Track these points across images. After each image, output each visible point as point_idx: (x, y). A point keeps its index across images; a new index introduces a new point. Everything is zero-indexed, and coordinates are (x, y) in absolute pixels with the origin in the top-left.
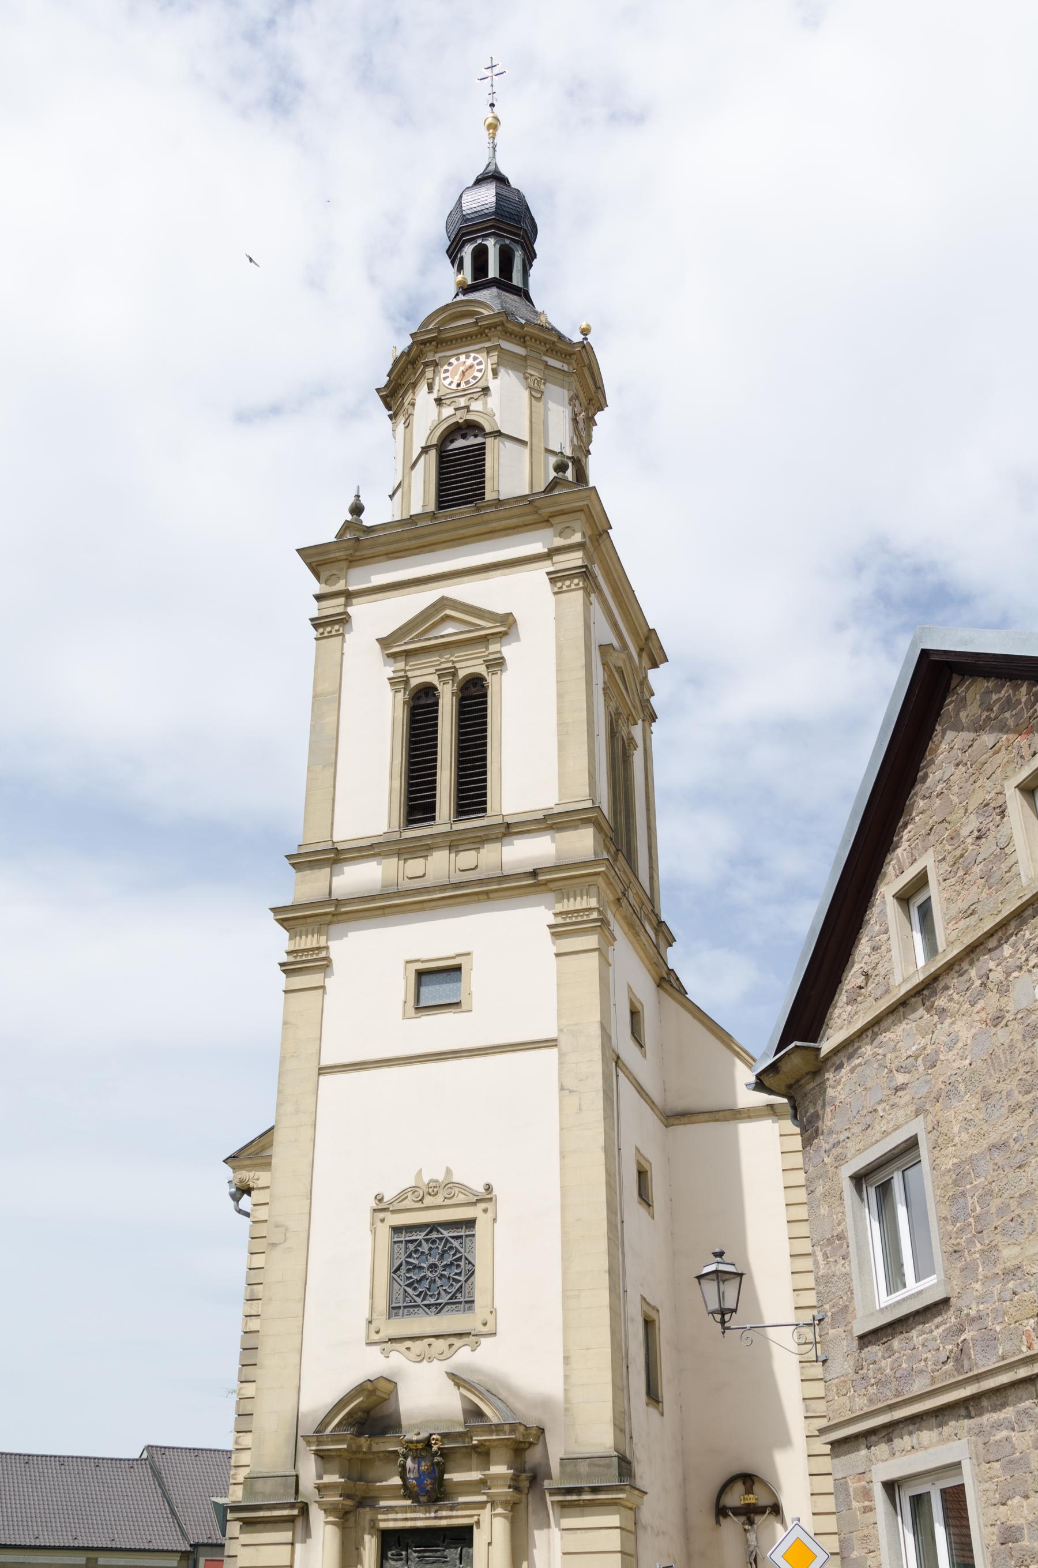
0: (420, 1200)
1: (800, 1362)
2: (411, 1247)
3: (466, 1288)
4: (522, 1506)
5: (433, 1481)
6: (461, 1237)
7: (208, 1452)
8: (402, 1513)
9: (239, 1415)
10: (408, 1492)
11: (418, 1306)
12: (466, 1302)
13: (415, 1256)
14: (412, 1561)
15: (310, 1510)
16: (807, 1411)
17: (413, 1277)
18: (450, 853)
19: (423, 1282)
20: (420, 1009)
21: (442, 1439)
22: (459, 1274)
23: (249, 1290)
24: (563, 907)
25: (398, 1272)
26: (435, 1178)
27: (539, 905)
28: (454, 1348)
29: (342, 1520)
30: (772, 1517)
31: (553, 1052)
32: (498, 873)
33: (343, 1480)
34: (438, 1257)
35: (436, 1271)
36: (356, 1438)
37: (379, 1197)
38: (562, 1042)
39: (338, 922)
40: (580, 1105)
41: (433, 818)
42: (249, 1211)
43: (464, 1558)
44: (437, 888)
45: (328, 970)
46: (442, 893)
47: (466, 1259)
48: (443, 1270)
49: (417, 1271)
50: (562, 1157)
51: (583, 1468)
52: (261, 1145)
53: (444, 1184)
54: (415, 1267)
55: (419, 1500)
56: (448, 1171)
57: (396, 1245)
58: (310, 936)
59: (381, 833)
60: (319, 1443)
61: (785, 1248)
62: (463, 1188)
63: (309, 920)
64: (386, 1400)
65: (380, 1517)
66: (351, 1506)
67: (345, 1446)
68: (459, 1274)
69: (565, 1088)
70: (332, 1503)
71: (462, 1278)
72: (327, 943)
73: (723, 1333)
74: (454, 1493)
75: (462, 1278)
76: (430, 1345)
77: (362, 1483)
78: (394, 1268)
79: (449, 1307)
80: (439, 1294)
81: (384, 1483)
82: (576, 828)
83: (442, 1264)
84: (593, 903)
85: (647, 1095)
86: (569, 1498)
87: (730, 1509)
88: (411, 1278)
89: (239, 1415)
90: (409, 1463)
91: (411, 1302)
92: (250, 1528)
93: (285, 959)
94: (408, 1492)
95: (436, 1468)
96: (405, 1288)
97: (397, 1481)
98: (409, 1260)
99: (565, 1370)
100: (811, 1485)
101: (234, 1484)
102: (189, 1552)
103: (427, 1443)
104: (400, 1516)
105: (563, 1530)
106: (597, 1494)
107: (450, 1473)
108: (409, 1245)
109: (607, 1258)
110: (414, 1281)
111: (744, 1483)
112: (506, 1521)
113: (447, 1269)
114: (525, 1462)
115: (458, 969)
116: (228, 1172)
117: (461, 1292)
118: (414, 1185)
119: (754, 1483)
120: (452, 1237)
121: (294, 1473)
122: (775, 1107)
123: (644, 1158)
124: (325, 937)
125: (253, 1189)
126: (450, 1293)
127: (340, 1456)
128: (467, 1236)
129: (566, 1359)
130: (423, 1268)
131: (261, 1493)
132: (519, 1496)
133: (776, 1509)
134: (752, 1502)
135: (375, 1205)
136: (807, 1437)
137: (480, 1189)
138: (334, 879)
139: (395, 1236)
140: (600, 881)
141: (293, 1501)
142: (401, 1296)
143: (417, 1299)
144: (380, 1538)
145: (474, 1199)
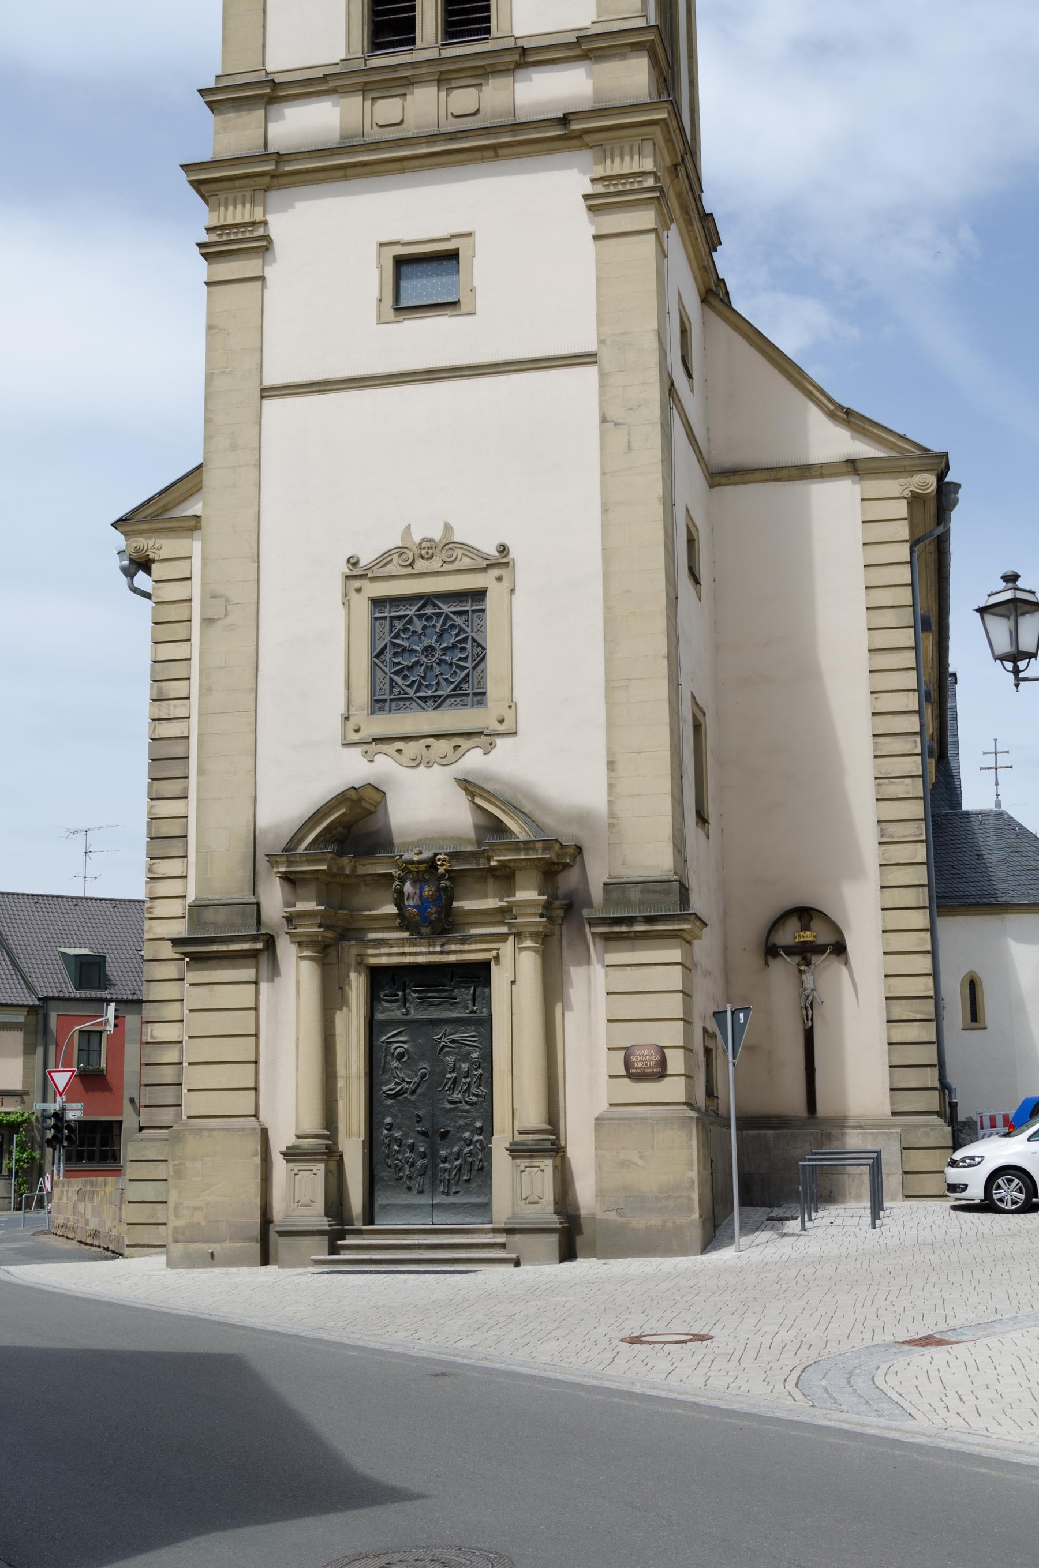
0: (410, 565)
1: (876, 778)
2: (399, 625)
3: (475, 677)
4: (554, 939)
5: (439, 909)
6: (466, 612)
7: (50, 898)
8: (398, 946)
9: (151, 838)
10: (404, 921)
11: (411, 699)
12: (475, 694)
13: (404, 636)
14: (411, 1003)
15: (277, 944)
16: (882, 836)
17: (402, 662)
18: (438, 91)
19: (415, 669)
20: (402, 310)
21: (450, 859)
22: (465, 659)
23: (155, 688)
24: (605, 170)
25: (382, 656)
26: (429, 536)
27: (569, 167)
28: (461, 751)
29: (322, 955)
30: (833, 957)
31: (592, 371)
32: (510, 120)
33: (323, 908)
34: (435, 637)
35: (433, 656)
36: (337, 858)
37: (352, 561)
38: (605, 357)
39: (280, 187)
40: (629, 442)
41: (412, 41)
42: (150, 591)
43: (478, 999)
44: (424, 140)
45: (268, 255)
46: (430, 147)
47: (474, 640)
48: (443, 654)
49: (406, 655)
50: (605, 510)
51: (635, 894)
52: (161, 504)
53: (443, 544)
54: (405, 650)
55: (420, 931)
56: (448, 528)
57: (377, 623)
58: (239, 207)
59: (338, 61)
60: (290, 863)
61: (862, 641)
62: (469, 549)
63: (237, 183)
64: (372, 813)
65: (370, 951)
66: (331, 938)
67: (325, 867)
68: (465, 659)
69: (608, 419)
70: (308, 935)
71: (469, 665)
72: (264, 216)
73: (1017, 685)
74: (459, 924)
75: (469, 665)
76: (428, 747)
77: (345, 912)
78: (377, 651)
79: (453, 700)
80: (438, 684)
81: (373, 912)
82: (623, 57)
83: (441, 647)
84: (648, 165)
85: (696, 440)
86: (617, 929)
87: (782, 947)
88: (399, 663)
89: (151, 838)
90: (408, 888)
91: (400, 693)
92: (199, 965)
93: (205, 238)
94: (406, 923)
95: (442, 893)
96: (392, 676)
97: (391, 909)
98: (396, 641)
99: (609, 778)
100: (884, 921)
101: (150, 919)
102: (38, 1006)
103: (432, 864)
104: (395, 950)
105: (607, 966)
106: (653, 925)
107: (459, 900)
108: (396, 622)
109: (666, 640)
110: (403, 668)
111: (800, 919)
112: (537, 956)
113: (448, 653)
114: (557, 888)
115: (453, 256)
116: (118, 539)
117: (468, 681)
118: (401, 545)
119: (812, 919)
120: (454, 613)
121: (254, 900)
122: (858, 464)
123: (693, 522)
124: (262, 208)
125: (153, 561)
126: (452, 683)
127: (317, 879)
128: (474, 611)
129: (611, 765)
130: (416, 651)
131: (212, 923)
132: (551, 927)
133: (840, 949)
134: (809, 939)
135: (347, 570)
136: (881, 865)
137: (492, 551)
138: (271, 126)
139: (377, 610)
140: (657, 131)
141: (255, 933)
142: (387, 687)
143: (408, 690)
144: (369, 976)
145: (485, 563)
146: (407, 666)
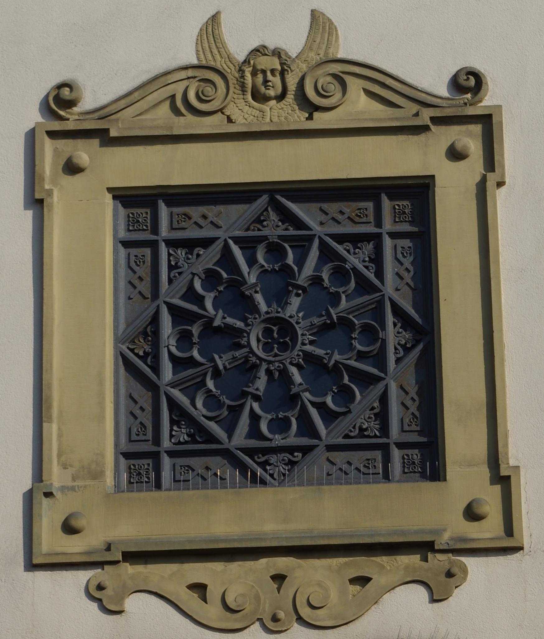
13: (260, 257)
34: (316, 321)
146: (211, 320)
